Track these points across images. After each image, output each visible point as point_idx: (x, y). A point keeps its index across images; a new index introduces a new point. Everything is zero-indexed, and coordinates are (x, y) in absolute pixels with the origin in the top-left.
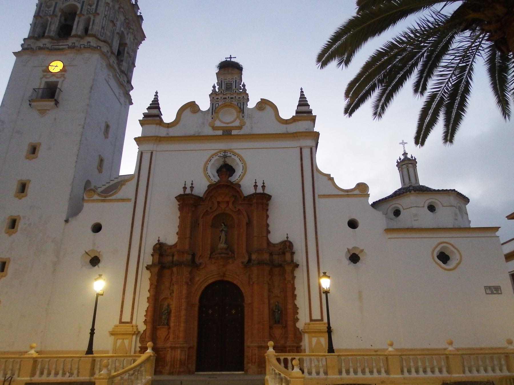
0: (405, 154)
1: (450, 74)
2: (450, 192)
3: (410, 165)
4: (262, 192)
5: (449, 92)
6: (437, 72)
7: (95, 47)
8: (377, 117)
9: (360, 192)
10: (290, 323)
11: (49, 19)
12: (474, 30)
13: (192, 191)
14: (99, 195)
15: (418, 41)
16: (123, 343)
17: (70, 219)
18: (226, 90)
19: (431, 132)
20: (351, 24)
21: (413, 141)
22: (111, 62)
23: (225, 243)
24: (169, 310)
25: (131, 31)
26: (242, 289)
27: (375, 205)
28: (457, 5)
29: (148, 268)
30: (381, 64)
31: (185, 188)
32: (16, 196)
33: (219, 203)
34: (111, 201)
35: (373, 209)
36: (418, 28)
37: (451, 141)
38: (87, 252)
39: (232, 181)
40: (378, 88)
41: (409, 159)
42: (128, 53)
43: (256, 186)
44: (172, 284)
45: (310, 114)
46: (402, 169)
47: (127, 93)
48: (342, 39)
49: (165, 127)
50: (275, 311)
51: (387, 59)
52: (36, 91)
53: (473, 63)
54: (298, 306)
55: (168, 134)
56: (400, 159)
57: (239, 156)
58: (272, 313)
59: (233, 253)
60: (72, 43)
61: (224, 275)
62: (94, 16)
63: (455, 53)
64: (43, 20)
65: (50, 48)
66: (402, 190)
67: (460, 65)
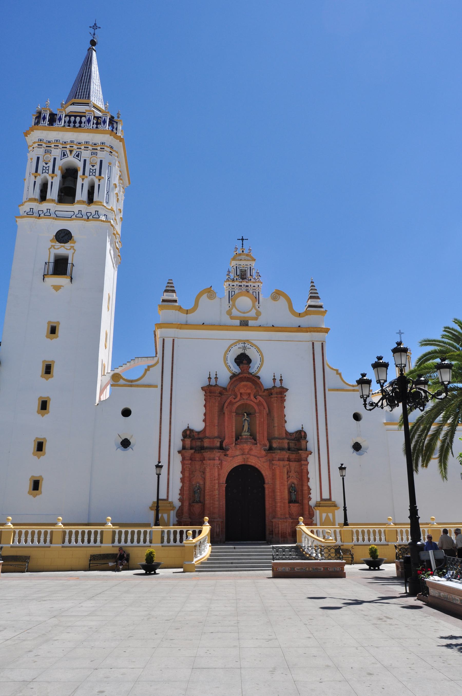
16: (327, 516)
43: (274, 380)
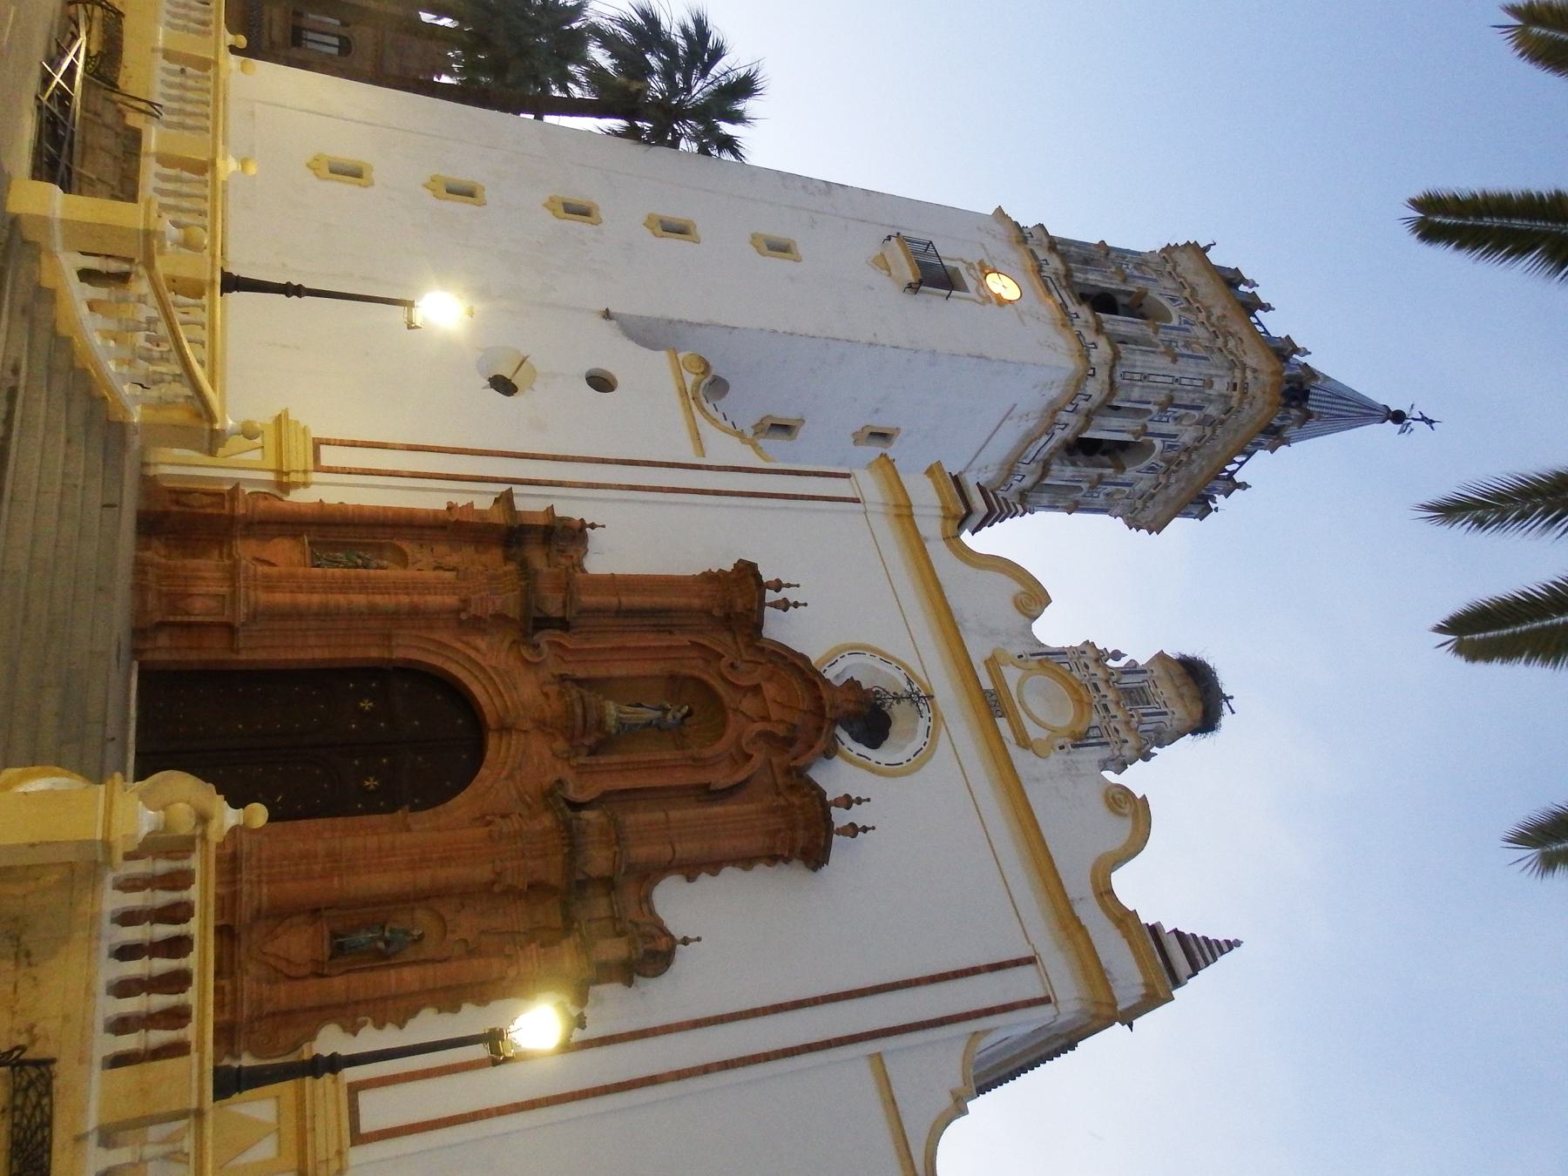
10: (338, 986)
13: (775, 605)
17: (614, 323)
18: (1121, 689)
23: (621, 723)
25: (1163, 480)
31: (778, 586)
42: (1100, 480)
45: (1169, 983)
50: (384, 931)
58: (378, 908)
59: (593, 752)
60: (1076, 314)
61: (505, 729)
64: (1102, 259)
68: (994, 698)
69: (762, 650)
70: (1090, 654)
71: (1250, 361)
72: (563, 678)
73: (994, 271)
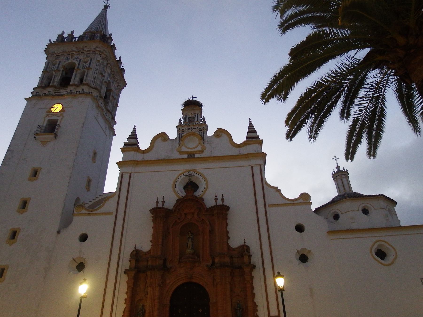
0: (338, 167)
1: (367, 103)
2: (379, 196)
3: (343, 176)
4: (221, 204)
5: (368, 116)
6: (357, 101)
7: (88, 93)
8: (312, 139)
9: (303, 200)
11: (54, 73)
12: (382, 69)
13: (163, 204)
14: (86, 210)
15: (339, 79)
17: (61, 230)
19: (358, 149)
20: (286, 71)
21: (344, 157)
22: (100, 104)
23: (192, 249)
24: (143, 311)
25: (116, 80)
26: (207, 290)
27: (317, 211)
28: (367, 51)
29: (126, 272)
30: (312, 99)
31: (157, 202)
32: (18, 211)
33: (186, 214)
34: (96, 214)
35: (314, 214)
36: (338, 70)
37: (374, 156)
38: (74, 258)
39: (196, 196)
40: (312, 116)
41: (341, 171)
42: (113, 96)
43: (216, 199)
44: (146, 287)
45: (257, 139)
46: (337, 179)
47: (112, 126)
48: (279, 81)
49: (142, 153)
51: (316, 94)
52: (41, 127)
53: (384, 94)
54: (257, 304)
55: (143, 159)
56: (334, 171)
57: (201, 174)
60: (70, 90)
62: (88, 70)
63: (370, 87)
65: (53, 94)
66: (339, 197)
67: (375, 95)
68: (190, 155)
69: (175, 210)
70: (180, 127)
71: (93, 47)
72: (179, 262)
73: (51, 109)
